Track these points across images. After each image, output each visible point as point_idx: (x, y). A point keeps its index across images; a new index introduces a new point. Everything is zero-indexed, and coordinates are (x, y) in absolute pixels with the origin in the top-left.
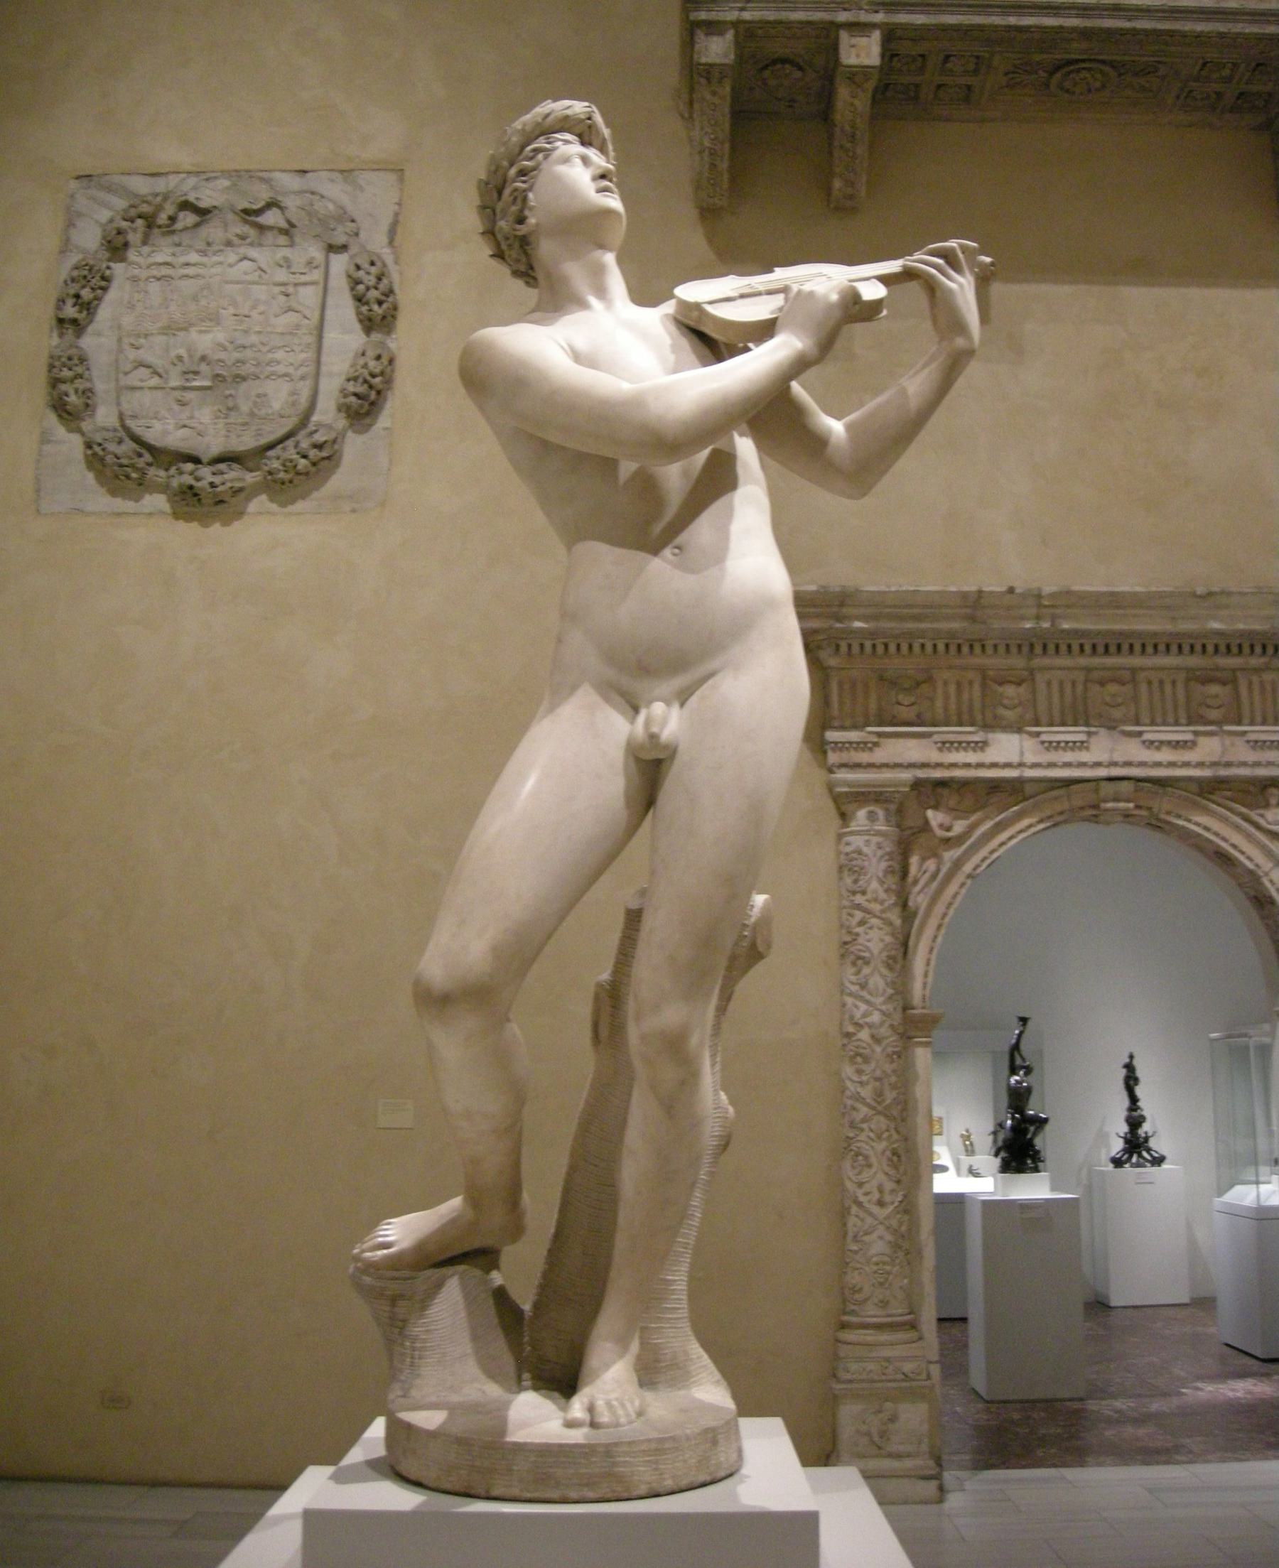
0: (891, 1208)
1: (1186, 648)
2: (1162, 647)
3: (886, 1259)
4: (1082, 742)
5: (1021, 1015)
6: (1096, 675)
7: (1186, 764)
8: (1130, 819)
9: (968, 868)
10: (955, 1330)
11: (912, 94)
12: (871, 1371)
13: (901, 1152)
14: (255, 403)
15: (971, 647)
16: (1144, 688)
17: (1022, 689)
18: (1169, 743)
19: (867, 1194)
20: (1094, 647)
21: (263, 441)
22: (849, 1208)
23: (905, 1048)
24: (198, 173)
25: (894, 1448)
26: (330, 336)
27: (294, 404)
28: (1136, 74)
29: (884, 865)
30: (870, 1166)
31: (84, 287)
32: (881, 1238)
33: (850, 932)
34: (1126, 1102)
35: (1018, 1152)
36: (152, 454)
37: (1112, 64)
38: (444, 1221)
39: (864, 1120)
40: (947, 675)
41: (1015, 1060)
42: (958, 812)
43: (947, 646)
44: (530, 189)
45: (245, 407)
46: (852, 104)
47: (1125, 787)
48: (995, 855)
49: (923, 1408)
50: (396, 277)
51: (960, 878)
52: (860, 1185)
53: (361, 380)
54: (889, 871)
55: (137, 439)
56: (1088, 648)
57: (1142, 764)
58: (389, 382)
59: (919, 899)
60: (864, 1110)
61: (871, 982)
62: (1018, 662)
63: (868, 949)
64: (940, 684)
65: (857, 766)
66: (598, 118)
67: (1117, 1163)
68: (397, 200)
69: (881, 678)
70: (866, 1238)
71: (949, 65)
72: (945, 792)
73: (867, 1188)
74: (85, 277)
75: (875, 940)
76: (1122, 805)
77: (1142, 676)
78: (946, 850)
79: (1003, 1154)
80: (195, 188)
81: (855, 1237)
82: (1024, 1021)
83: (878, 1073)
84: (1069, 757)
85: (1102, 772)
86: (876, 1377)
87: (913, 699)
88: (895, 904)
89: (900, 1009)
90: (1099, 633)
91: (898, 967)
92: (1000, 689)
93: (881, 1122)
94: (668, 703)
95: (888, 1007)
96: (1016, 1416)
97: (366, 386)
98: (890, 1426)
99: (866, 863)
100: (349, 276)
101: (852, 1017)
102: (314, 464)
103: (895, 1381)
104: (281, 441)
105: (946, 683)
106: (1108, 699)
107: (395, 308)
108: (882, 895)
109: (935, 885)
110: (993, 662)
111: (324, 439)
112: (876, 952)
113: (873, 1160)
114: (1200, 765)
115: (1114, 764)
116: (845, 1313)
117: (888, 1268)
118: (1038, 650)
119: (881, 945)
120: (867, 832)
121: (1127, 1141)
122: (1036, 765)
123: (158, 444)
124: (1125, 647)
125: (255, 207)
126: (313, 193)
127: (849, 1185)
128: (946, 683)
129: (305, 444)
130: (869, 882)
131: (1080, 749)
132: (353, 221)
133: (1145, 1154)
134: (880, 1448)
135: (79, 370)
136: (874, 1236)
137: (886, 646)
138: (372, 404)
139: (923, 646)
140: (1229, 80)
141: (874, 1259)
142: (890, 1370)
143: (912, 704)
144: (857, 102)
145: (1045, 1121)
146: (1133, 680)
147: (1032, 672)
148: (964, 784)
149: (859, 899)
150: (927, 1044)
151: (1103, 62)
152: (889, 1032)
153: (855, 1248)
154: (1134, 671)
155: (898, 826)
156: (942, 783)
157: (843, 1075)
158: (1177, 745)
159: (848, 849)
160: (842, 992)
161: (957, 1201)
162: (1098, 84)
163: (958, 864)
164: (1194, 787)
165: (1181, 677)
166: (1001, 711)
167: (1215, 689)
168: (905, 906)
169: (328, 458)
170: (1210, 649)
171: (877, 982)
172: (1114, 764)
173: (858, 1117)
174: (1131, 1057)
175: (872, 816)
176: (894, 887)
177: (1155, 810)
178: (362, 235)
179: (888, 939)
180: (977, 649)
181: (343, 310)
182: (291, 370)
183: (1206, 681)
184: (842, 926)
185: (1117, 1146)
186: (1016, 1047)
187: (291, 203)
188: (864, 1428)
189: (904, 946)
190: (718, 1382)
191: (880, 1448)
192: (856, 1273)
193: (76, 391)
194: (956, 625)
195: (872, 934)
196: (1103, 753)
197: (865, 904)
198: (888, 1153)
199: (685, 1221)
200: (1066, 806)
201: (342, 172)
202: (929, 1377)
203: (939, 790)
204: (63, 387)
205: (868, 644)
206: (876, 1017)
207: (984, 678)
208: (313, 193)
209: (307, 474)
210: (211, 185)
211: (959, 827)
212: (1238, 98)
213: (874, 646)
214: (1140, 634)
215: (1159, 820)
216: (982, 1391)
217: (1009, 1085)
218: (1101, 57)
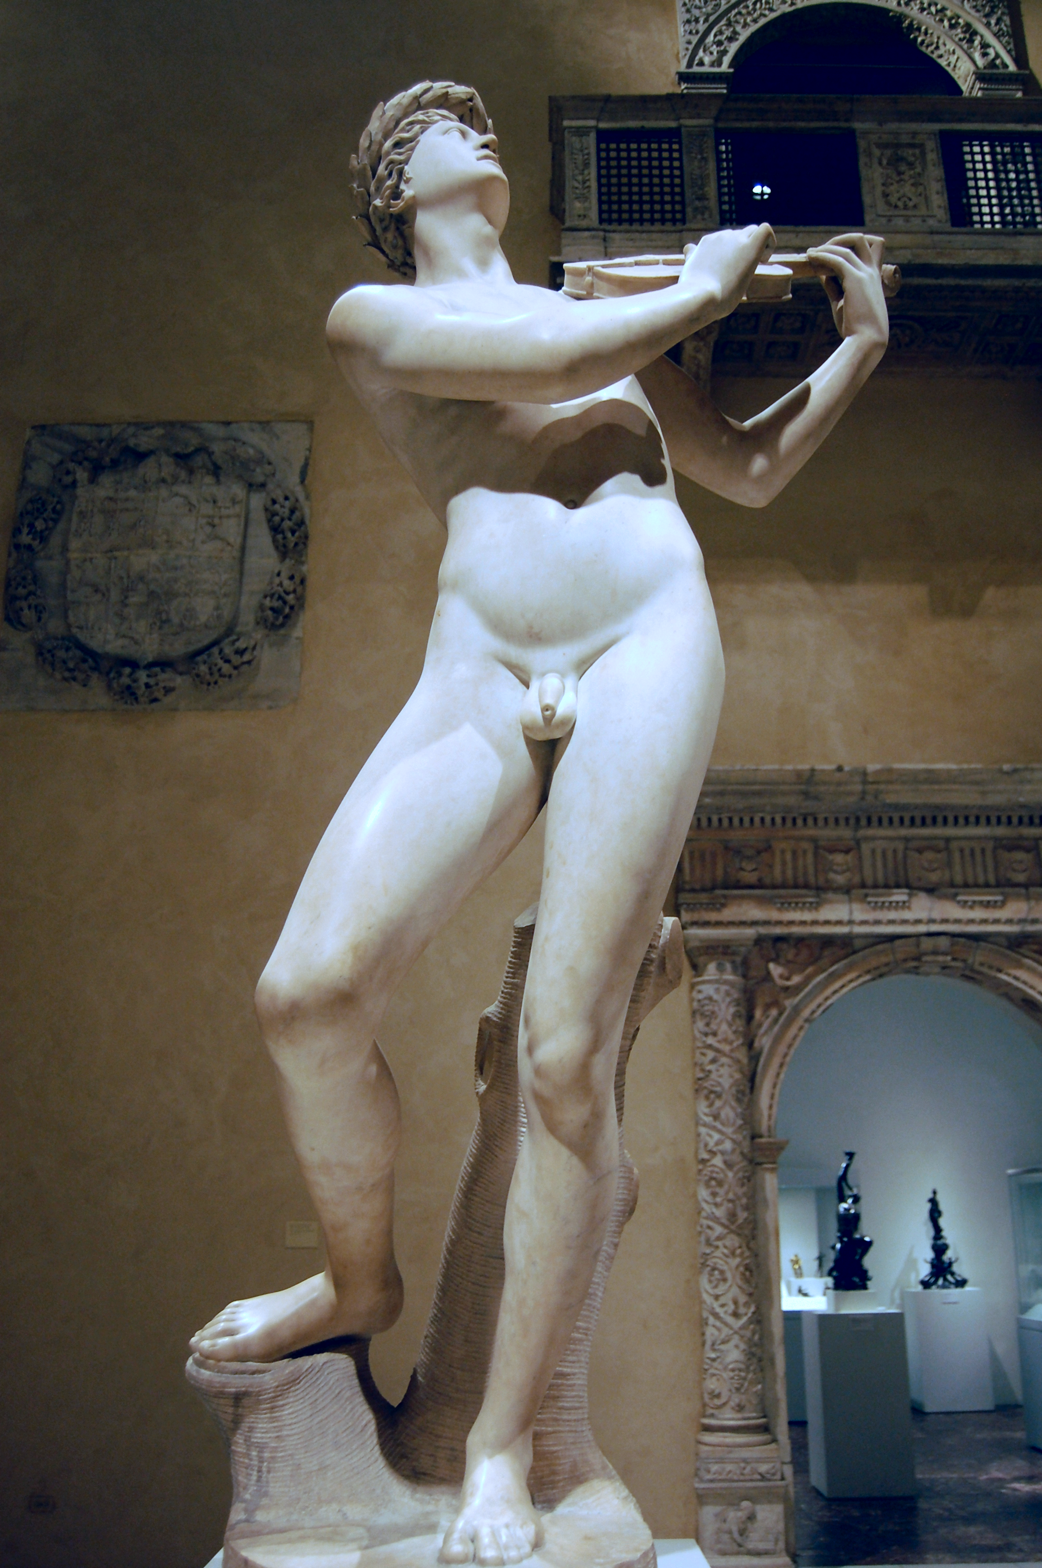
0: (745, 1319)
1: (994, 820)
2: (972, 819)
3: (742, 1366)
4: (904, 902)
5: (848, 1151)
7: (996, 921)
8: (947, 971)
9: (806, 1013)
12: (730, 1472)
13: (754, 1268)
14: (185, 616)
15: (805, 820)
16: (957, 855)
17: (849, 857)
18: (981, 902)
19: (723, 1306)
21: (192, 648)
22: (707, 1318)
23: (754, 1173)
24: (136, 424)
25: (751, 1546)
26: (253, 561)
27: (219, 617)
29: (732, 1010)
30: (725, 1280)
31: (36, 519)
32: (737, 1346)
33: (703, 1070)
35: (848, 1269)
38: (302, 1303)
39: (718, 1238)
40: (783, 845)
41: (842, 1187)
42: (793, 967)
44: (406, 162)
45: (176, 620)
47: (943, 942)
48: (829, 1002)
50: (307, 511)
51: (799, 1022)
52: (717, 1297)
53: (276, 596)
54: (736, 1015)
56: (907, 821)
57: (957, 921)
58: (301, 599)
59: (764, 1042)
60: (719, 1230)
61: (723, 1115)
62: (845, 833)
63: (719, 1084)
64: (778, 853)
65: (706, 924)
66: (479, 101)
67: (926, 1285)
68: (308, 446)
69: (726, 848)
70: (722, 1347)
71: (779, 324)
72: (785, 946)
73: (722, 1300)
74: (38, 510)
75: (725, 1076)
76: (941, 958)
77: (954, 845)
78: (787, 998)
80: (134, 435)
81: (713, 1345)
82: (851, 1155)
83: (731, 1196)
84: (892, 915)
85: (922, 928)
86: (735, 1477)
87: (754, 866)
88: (742, 1044)
89: (748, 1139)
90: (917, 807)
91: (746, 1099)
92: (831, 857)
93: (732, 1241)
94: (563, 675)
95: (738, 1137)
96: (856, 1513)
97: (280, 602)
98: (749, 1525)
99: (716, 1009)
101: (706, 1145)
102: (236, 668)
103: (751, 1480)
104: (208, 648)
106: (926, 865)
107: (306, 537)
108: (731, 1036)
109: (776, 1028)
110: (827, 833)
111: (244, 646)
112: (727, 1085)
113: (729, 1275)
114: (1009, 921)
115: (931, 921)
116: (705, 1416)
117: (743, 1374)
119: (731, 1081)
120: (717, 981)
123: (100, 651)
124: (940, 819)
125: (186, 452)
126: (235, 440)
127: (705, 1296)
128: (783, 852)
129: (228, 650)
130: (719, 1025)
131: (903, 908)
132: (270, 463)
133: (949, 1277)
134: (740, 1545)
135: (32, 588)
137: (730, 819)
138: (287, 617)
141: (731, 1366)
142: (747, 1470)
143: (754, 870)
144: (700, 357)
145: (870, 1243)
147: (858, 842)
148: (800, 941)
149: (710, 1040)
150: (773, 1170)
152: (740, 1158)
153: (713, 1355)
154: (948, 840)
155: (744, 976)
157: (700, 1198)
158: (987, 905)
159: (700, 996)
160: (697, 1124)
161: (794, 1318)
162: (907, 339)
163: (797, 1010)
165: (990, 845)
166: (832, 876)
167: (1020, 855)
168: (750, 1045)
169: (249, 662)
170: (1015, 820)
171: (728, 1113)
172: (931, 921)
174: (935, 1193)
175: (720, 968)
176: (741, 1029)
177: (970, 961)
178: (278, 476)
179: (737, 1076)
180: (810, 821)
181: (262, 538)
182: (216, 588)
184: (696, 1064)
185: (925, 1270)
186: (843, 1178)
187: (217, 448)
188: (725, 1526)
190: (625, 1498)
191: (740, 1545)
192: (714, 1378)
193: (30, 607)
195: (722, 1071)
196: (921, 913)
197: (716, 1045)
198: (742, 1269)
199: (587, 1301)
200: (890, 958)
201: (260, 423)
202: (783, 1479)
203: (779, 945)
204: (18, 604)
205: (715, 819)
206: (728, 1145)
207: (817, 848)
208: (235, 440)
209: (230, 676)
210: (148, 432)
211: (796, 979)
213: (720, 820)
214: (952, 807)
215: (972, 970)
216: (823, 1488)
218: (910, 313)
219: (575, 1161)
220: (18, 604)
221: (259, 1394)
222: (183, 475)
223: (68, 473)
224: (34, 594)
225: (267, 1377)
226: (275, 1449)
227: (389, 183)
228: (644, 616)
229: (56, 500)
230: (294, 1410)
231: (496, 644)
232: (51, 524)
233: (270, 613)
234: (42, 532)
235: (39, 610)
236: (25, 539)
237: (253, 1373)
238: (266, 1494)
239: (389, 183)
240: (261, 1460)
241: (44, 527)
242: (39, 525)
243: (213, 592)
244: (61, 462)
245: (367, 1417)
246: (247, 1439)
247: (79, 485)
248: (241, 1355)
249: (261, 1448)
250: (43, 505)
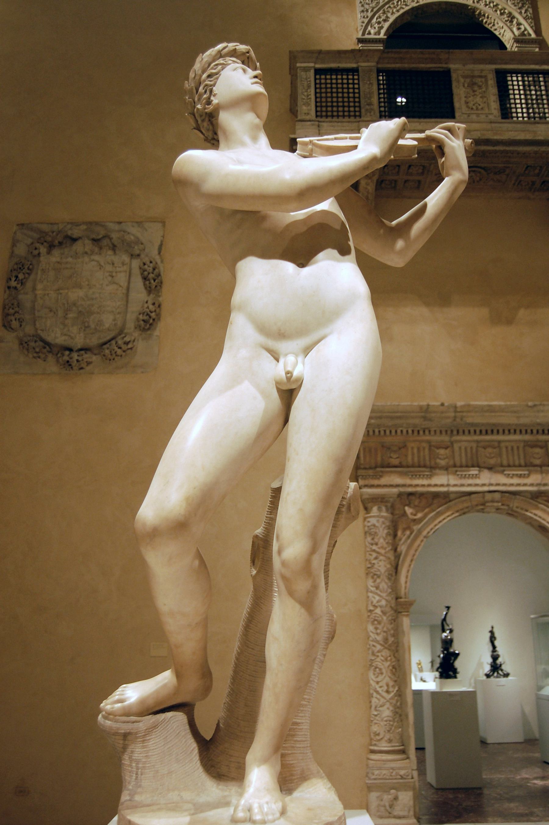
0: (392, 694)
1: (524, 432)
2: (512, 431)
3: (391, 719)
4: (476, 475)
5: (447, 605)
6: (482, 444)
9: (425, 533)
10: (421, 752)
11: (393, 185)
12: (385, 774)
13: (397, 667)
15: (424, 431)
16: (504, 450)
17: (447, 451)
18: (517, 475)
19: (381, 687)
20: (481, 431)
22: (372, 694)
23: (397, 617)
24: (72, 223)
25: (396, 813)
26: (133, 295)
28: (495, 173)
29: (386, 531)
30: (382, 673)
31: (19, 273)
32: (388, 708)
33: (370, 563)
34: (491, 648)
35: (447, 668)
36: (50, 348)
37: (484, 168)
39: (379, 652)
40: (413, 445)
42: (418, 509)
43: (413, 431)
44: (214, 85)
45: (93, 326)
46: (366, 188)
47: (497, 496)
48: (437, 527)
49: (410, 794)
50: (162, 269)
51: (421, 538)
52: (378, 683)
53: (146, 314)
54: (388, 534)
55: (43, 340)
56: (478, 432)
57: (505, 485)
58: (159, 315)
59: (402, 548)
60: (379, 647)
62: (445, 438)
63: (379, 570)
64: (410, 449)
65: (372, 486)
66: (252, 53)
67: (488, 676)
69: (383, 446)
70: (381, 709)
71: (410, 171)
73: (380, 684)
74: (20, 268)
75: (382, 566)
76: (496, 504)
77: (503, 445)
78: (415, 525)
79: (440, 670)
80: (71, 229)
81: (376, 707)
82: (448, 608)
83: (385, 629)
84: (470, 481)
85: (486, 489)
86: (387, 777)
87: (397, 456)
88: (391, 550)
90: (483, 425)
91: (393, 578)
92: (438, 451)
93: (386, 653)
94: (297, 355)
95: (389, 598)
97: (148, 317)
98: (395, 802)
99: (377, 531)
100: (140, 268)
101: (372, 602)
102: (124, 351)
103: (396, 779)
104: (110, 341)
105: (412, 448)
106: (488, 455)
107: (161, 283)
108: (385, 545)
109: (409, 541)
110: (436, 439)
113: (384, 671)
114: (532, 485)
115: (491, 485)
116: (371, 745)
118: (455, 432)
119: (385, 568)
120: (378, 516)
121: (492, 666)
122: (455, 485)
123: (53, 342)
124: (495, 431)
127: (371, 682)
128: (412, 448)
129: (120, 342)
130: (379, 539)
132: (142, 244)
133: (500, 672)
134: (390, 813)
135: (17, 309)
136: (385, 707)
137: (385, 431)
138: (151, 325)
139: (402, 431)
140: (538, 175)
141: (385, 719)
143: (397, 458)
144: (369, 188)
145: (458, 654)
146: (499, 446)
147: (452, 443)
149: (374, 547)
150: (407, 615)
151: (480, 167)
153: (376, 713)
154: (499, 442)
156: (411, 494)
157: (369, 630)
158: (520, 476)
159: (369, 524)
161: (418, 693)
163: (420, 531)
164: (529, 496)
165: (522, 445)
166: (438, 461)
167: (537, 450)
168: (395, 550)
169: (131, 349)
170: (535, 431)
171: (383, 586)
172: (491, 485)
173: (376, 650)
174: (492, 628)
175: (380, 509)
176: (390, 541)
177: (511, 506)
179: (389, 566)
180: (427, 432)
181: (138, 283)
183: (532, 447)
185: (487, 668)
186: (444, 620)
187: (114, 236)
188: (382, 803)
189: (396, 569)
191: (390, 813)
192: (376, 725)
193: (16, 320)
194: (417, 421)
195: (381, 563)
196: (485, 480)
197: (377, 550)
198: (391, 668)
200: (469, 504)
203: (410, 497)
205: (377, 431)
206: (383, 603)
207: (430, 446)
209: (121, 356)
211: (419, 515)
212: (542, 184)
213: (379, 432)
215: (512, 510)
217: (441, 637)
219: (303, 611)
220: (10, 318)
221: (136, 733)
222: (96, 250)
223: (36, 249)
224: (18, 313)
225: (141, 724)
226: (145, 763)
227: (205, 96)
228: (340, 324)
229: (29, 263)
230: (155, 742)
231: (261, 339)
232: (27, 276)
233: (142, 322)
234: (22, 280)
235: (21, 321)
236: (13, 283)
237: (133, 722)
238: (140, 786)
239: (205, 96)
240: (138, 769)
241: (23, 277)
242: (21, 276)
243: (113, 312)
244: (32, 243)
245: (193, 745)
246: (130, 757)
247: (41, 255)
248: (127, 713)
249: (138, 762)
250: (23, 266)
